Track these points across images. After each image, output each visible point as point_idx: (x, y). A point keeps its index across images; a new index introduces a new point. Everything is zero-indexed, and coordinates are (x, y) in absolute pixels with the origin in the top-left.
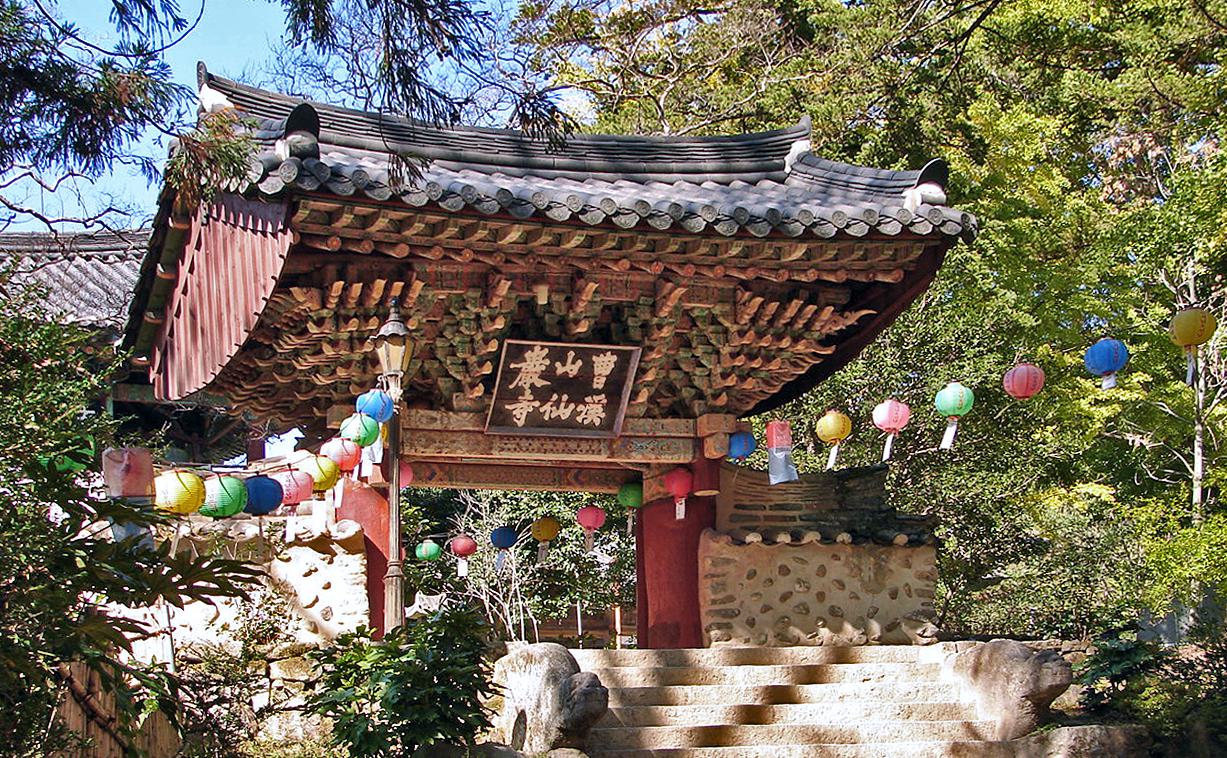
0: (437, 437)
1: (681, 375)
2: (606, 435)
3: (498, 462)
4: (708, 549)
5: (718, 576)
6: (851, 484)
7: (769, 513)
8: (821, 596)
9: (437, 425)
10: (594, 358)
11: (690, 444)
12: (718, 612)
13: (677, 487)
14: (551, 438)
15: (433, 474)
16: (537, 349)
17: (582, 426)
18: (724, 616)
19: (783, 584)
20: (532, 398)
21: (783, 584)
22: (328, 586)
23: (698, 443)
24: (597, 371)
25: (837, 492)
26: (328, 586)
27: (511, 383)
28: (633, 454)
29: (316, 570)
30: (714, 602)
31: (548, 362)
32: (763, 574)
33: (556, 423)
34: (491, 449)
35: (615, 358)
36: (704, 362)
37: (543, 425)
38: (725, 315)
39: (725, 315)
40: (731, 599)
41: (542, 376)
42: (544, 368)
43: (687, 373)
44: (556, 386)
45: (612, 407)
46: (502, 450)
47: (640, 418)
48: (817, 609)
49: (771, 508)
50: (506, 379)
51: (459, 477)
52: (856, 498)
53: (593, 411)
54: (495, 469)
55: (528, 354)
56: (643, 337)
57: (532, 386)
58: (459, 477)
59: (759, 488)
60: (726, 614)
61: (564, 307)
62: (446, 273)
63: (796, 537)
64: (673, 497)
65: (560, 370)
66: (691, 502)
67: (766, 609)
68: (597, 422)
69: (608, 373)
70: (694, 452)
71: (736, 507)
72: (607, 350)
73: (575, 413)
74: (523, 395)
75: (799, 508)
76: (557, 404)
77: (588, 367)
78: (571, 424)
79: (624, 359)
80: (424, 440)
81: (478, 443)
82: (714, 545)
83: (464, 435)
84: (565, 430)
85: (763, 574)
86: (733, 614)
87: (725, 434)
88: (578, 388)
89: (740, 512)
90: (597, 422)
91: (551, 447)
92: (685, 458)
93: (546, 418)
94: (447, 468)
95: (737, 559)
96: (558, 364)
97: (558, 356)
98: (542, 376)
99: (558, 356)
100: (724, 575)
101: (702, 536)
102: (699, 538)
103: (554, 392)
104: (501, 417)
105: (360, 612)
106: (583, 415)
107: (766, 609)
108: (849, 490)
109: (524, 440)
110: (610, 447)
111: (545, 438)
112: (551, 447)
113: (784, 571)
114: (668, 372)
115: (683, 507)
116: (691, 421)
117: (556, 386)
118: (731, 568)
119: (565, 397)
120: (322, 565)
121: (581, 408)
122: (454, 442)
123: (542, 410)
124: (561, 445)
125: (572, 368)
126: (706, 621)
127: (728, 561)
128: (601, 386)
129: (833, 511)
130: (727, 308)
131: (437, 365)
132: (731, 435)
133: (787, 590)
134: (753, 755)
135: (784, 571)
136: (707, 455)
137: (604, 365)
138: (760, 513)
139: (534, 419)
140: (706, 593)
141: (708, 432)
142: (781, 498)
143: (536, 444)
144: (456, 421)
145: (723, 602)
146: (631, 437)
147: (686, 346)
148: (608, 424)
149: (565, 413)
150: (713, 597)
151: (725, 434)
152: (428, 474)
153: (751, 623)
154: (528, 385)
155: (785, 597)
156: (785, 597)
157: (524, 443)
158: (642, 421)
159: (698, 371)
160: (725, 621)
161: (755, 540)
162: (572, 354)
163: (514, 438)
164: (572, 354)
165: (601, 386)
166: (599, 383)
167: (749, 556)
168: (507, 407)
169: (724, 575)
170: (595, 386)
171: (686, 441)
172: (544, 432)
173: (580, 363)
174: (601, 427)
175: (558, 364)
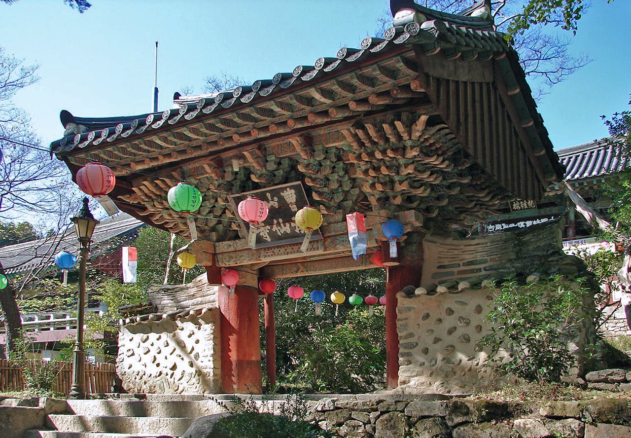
0: (232, 255)
3: (342, 255)
6: (527, 238)
7: (462, 268)
8: (479, 328)
9: (232, 249)
14: (290, 245)
15: (298, 270)
19: (449, 322)
21: (449, 322)
24: (288, 201)
25: (515, 246)
28: (338, 246)
29: (193, 333)
32: (434, 316)
34: (260, 257)
35: (293, 191)
37: (280, 238)
46: (266, 256)
48: (476, 338)
49: (464, 264)
51: (312, 268)
52: (531, 248)
58: (312, 268)
59: (456, 252)
62: (199, 167)
63: (453, 288)
67: (437, 340)
69: (294, 200)
72: (287, 187)
75: (485, 262)
77: (282, 200)
83: (247, 252)
84: (294, 239)
85: (434, 316)
89: (443, 270)
91: (291, 250)
95: (415, 306)
100: (407, 319)
105: (209, 355)
107: (437, 340)
108: (525, 243)
109: (276, 249)
112: (291, 250)
113: (450, 312)
119: (281, 220)
120: (196, 331)
122: (241, 256)
129: (510, 260)
133: (452, 326)
134: (113, 437)
135: (450, 312)
137: (290, 196)
138: (455, 270)
141: (221, 251)
142: (472, 256)
143: (282, 250)
152: (296, 269)
153: (426, 351)
155: (450, 332)
156: (450, 332)
157: (276, 251)
163: (271, 248)
167: (423, 304)
169: (407, 319)
172: (283, 242)
173: (276, 199)
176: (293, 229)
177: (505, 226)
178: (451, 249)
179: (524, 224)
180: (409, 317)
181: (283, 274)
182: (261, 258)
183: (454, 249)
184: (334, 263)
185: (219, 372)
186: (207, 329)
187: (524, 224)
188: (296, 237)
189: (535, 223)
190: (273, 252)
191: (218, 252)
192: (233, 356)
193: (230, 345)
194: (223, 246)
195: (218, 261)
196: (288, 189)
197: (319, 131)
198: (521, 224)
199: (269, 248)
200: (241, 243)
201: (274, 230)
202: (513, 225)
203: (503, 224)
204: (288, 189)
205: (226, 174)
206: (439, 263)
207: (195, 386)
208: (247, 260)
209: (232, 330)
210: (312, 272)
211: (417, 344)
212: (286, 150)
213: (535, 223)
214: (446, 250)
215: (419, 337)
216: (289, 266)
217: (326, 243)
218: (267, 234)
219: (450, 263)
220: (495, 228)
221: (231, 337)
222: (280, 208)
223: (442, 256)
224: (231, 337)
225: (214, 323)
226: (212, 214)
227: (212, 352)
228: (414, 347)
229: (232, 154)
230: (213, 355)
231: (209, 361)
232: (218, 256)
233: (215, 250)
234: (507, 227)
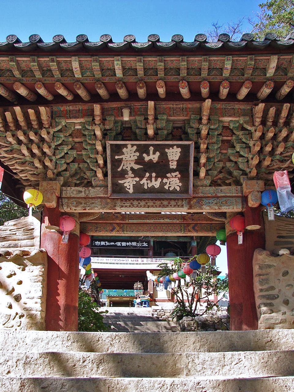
0: (83, 201)
1: (233, 165)
2: (184, 196)
4: (257, 260)
5: (263, 275)
9: (83, 195)
10: (166, 150)
11: (239, 200)
12: (263, 297)
13: (236, 226)
16: (129, 146)
17: (169, 192)
18: (268, 299)
20: (133, 176)
22: (20, 283)
23: (245, 199)
24: (170, 158)
26: (20, 283)
27: (119, 167)
28: (204, 207)
29: (15, 274)
30: (261, 290)
31: (138, 154)
33: (152, 190)
34: (115, 206)
35: (179, 150)
36: (242, 153)
37: (145, 192)
38: (246, 122)
39: (246, 122)
40: (272, 288)
41: (137, 162)
42: (136, 158)
43: (236, 163)
44: (145, 168)
45: (184, 178)
46: (122, 207)
47: (206, 186)
50: (115, 165)
53: (174, 182)
54: (148, 225)
55: (124, 150)
56: (198, 138)
57: (132, 169)
60: (269, 297)
61: (143, 123)
64: (236, 232)
65: (147, 158)
66: (247, 234)
68: (178, 189)
69: (177, 158)
70: (243, 205)
71: (278, 237)
73: (162, 184)
74: (128, 174)
76: (150, 178)
78: (161, 190)
79: (185, 150)
80: (75, 203)
81: (107, 204)
82: (260, 257)
83: (99, 200)
84: (159, 194)
86: (275, 297)
87: (258, 192)
88: (161, 169)
90: (178, 189)
91: (152, 204)
92: (238, 208)
93: (146, 187)
94: (122, 225)
95: (275, 264)
96: (145, 155)
97: (143, 150)
98: (137, 162)
99: (143, 150)
100: (267, 274)
101: (255, 253)
102: (254, 252)
103: (146, 171)
104: (118, 188)
106: (168, 185)
110: (189, 203)
111: (148, 199)
112: (152, 204)
114: (225, 163)
115: (241, 237)
116: (239, 187)
117: (145, 168)
118: (272, 270)
119: (154, 175)
120: (19, 272)
121: (165, 180)
122: (93, 203)
123: (142, 182)
124: (158, 203)
125: (154, 157)
126: (258, 301)
127: (269, 266)
128: (175, 167)
130: (247, 118)
131: (86, 165)
132: (262, 192)
136: (250, 205)
137: (174, 154)
139: (138, 188)
140: (257, 286)
141: (68, 195)
143: (142, 203)
144: (92, 192)
145: (267, 290)
146: (202, 197)
147: (232, 147)
148: (185, 190)
149: (156, 184)
150: (261, 288)
151: (258, 192)
152: (111, 228)
154: (129, 169)
158: (208, 188)
159: (240, 160)
160: (269, 301)
161: (285, 253)
162: (151, 149)
164: (151, 149)
165: (175, 167)
166: (173, 165)
167: (283, 263)
168: (120, 182)
169: (267, 274)
170: (171, 167)
171: (237, 199)
172: (147, 196)
173: (158, 154)
174: (181, 192)
175: (145, 155)
176: (162, 184)
177: (107, 244)
178: (289, 224)
179: (121, 244)
180: (269, 273)
181: (96, 231)
182: (117, 208)
183: (290, 224)
184: (152, 228)
185: (44, 315)
186: (34, 272)
187: (121, 244)
188: (164, 193)
189: (128, 244)
190: (132, 203)
191: (64, 196)
192: (61, 300)
193: (58, 289)
194: (72, 191)
195: (62, 205)
196: (175, 147)
197: (217, 105)
198: (119, 244)
199: (129, 199)
200: (95, 190)
201: (142, 182)
202: (113, 243)
203: (106, 242)
204: (175, 147)
205: (107, 122)
206: (278, 233)
207: (14, 329)
208: (99, 207)
209: (61, 275)
210: (128, 233)
211: (278, 296)
212: (178, 113)
213: (128, 244)
214: (284, 224)
215: (280, 290)
216: (104, 224)
217: (192, 203)
218: (132, 186)
219: (288, 235)
220: (100, 244)
221: (59, 281)
222: (158, 162)
223: (280, 228)
224: (59, 281)
225: (43, 264)
226: (64, 159)
227: (40, 294)
228: (276, 298)
229: (116, 106)
230: (41, 298)
231: (36, 303)
232: (63, 200)
233: (61, 193)
234: (109, 244)
